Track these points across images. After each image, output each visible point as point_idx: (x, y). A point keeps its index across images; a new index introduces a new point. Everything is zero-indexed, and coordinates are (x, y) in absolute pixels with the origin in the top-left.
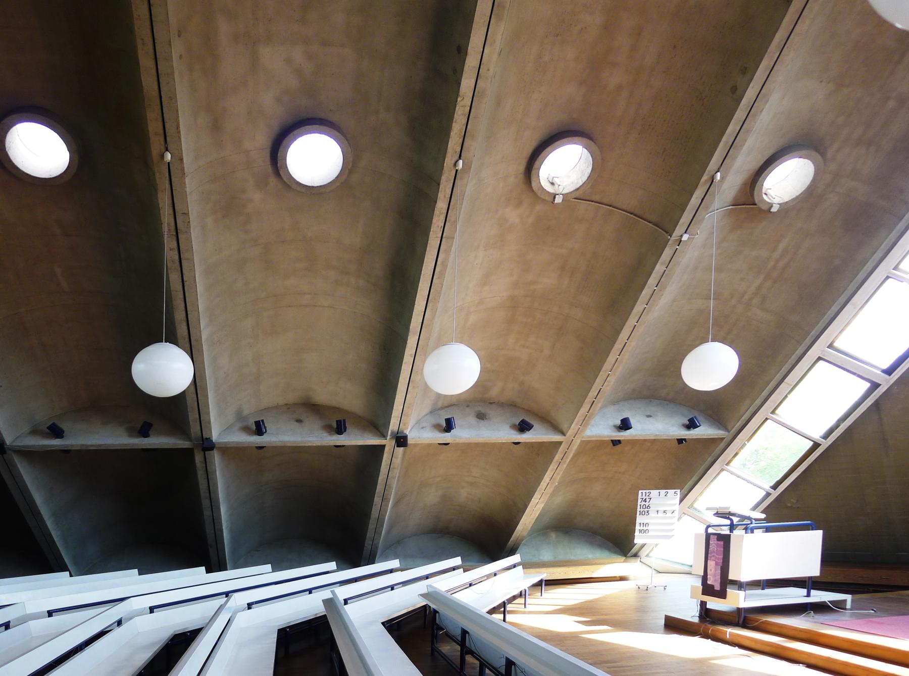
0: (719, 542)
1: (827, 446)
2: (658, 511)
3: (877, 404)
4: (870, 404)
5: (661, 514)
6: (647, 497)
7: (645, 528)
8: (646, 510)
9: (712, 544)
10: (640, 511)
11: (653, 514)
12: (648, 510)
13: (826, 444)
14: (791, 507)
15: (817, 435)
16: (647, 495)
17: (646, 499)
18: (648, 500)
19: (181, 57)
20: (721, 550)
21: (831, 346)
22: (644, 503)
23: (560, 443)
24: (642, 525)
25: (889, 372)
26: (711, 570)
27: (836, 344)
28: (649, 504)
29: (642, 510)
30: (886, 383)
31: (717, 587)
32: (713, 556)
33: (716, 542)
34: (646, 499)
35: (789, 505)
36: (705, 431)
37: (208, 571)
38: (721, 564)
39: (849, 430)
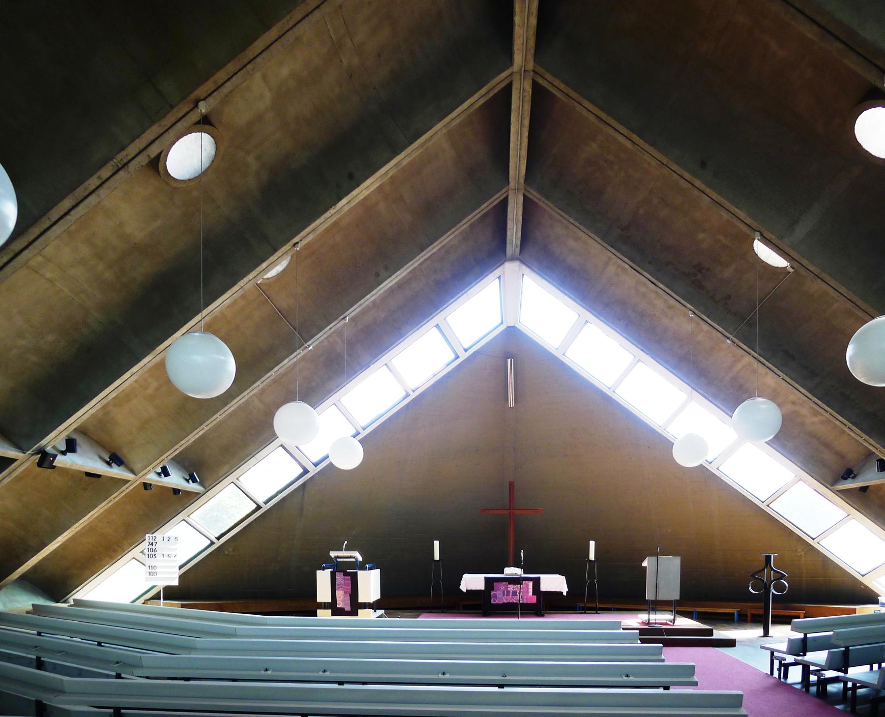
0: (346, 577)
1: (266, 509)
2: (163, 555)
3: (304, 485)
4: (300, 483)
5: (166, 558)
6: (154, 541)
7: (153, 571)
8: (153, 553)
9: (338, 579)
10: (148, 554)
11: (159, 557)
12: (155, 553)
13: (265, 508)
14: (228, 555)
15: (261, 500)
16: (154, 538)
17: (152, 543)
18: (154, 544)
19: (532, 14)
20: (349, 583)
21: (768, 506)
22: (150, 546)
23: (13, 461)
24: (151, 567)
25: (316, 465)
26: (340, 597)
27: (770, 506)
28: (155, 547)
29: (150, 553)
30: (313, 470)
31: (348, 608)
32: (341, 587)
33: (343, 577)
34: (152, 543)
35: (226, 553)
36: (176, 479)
37: (333, 614)
38: (350, 592)
39: (284, 500)
